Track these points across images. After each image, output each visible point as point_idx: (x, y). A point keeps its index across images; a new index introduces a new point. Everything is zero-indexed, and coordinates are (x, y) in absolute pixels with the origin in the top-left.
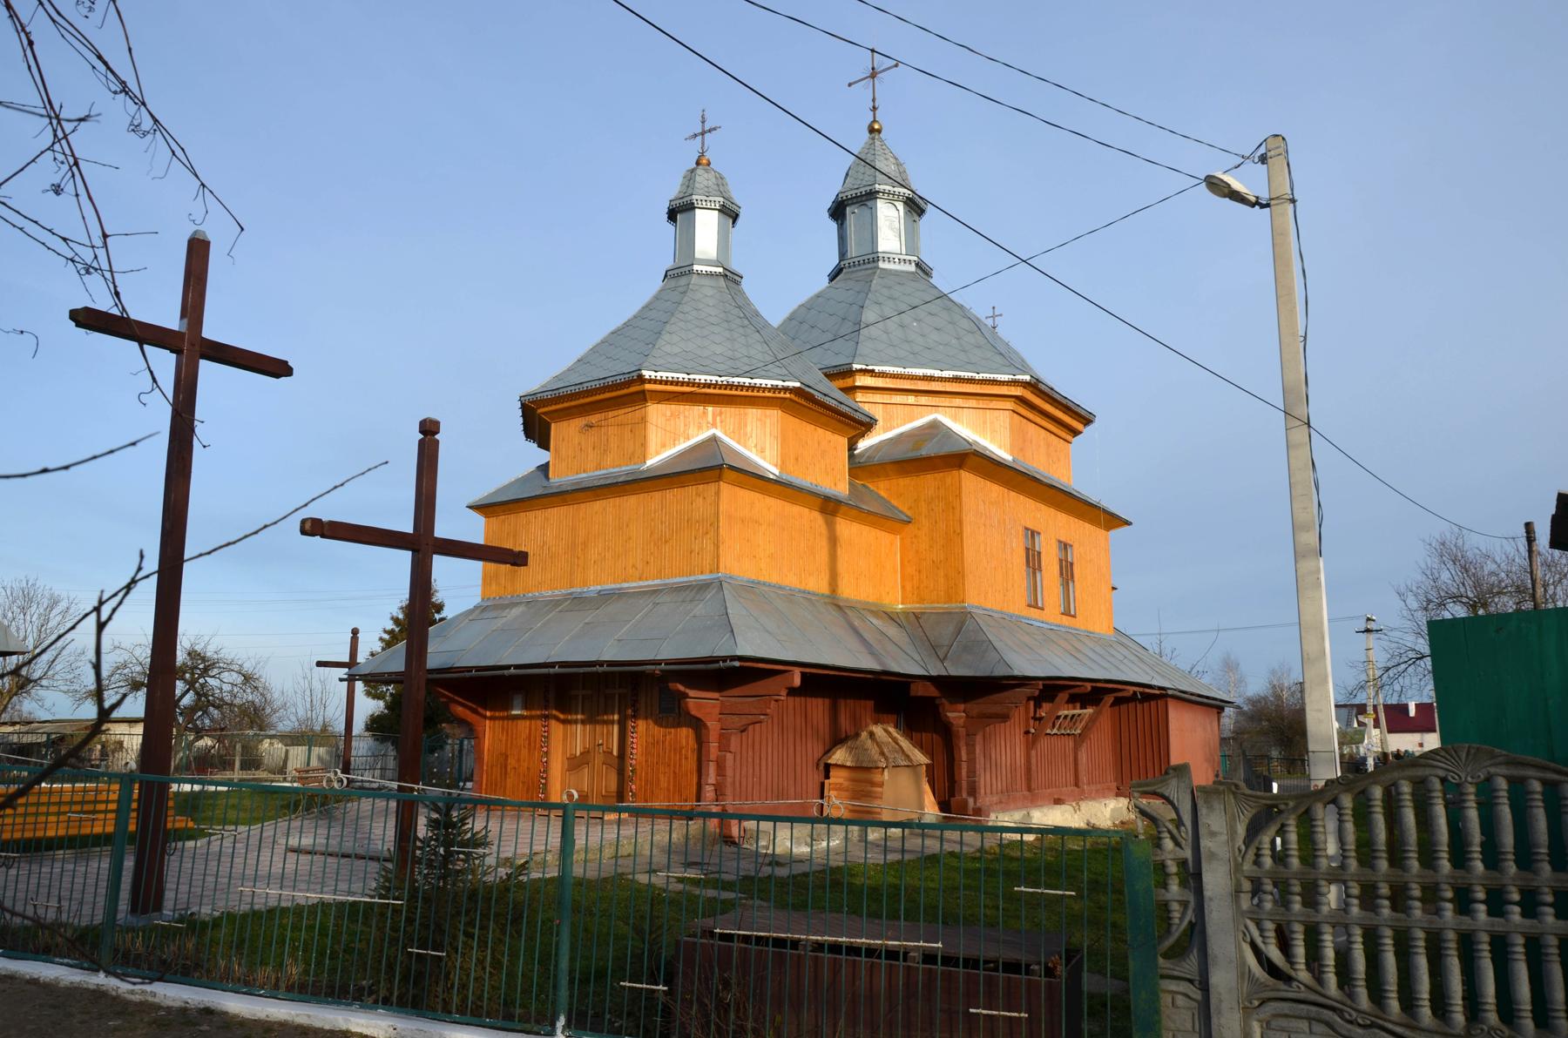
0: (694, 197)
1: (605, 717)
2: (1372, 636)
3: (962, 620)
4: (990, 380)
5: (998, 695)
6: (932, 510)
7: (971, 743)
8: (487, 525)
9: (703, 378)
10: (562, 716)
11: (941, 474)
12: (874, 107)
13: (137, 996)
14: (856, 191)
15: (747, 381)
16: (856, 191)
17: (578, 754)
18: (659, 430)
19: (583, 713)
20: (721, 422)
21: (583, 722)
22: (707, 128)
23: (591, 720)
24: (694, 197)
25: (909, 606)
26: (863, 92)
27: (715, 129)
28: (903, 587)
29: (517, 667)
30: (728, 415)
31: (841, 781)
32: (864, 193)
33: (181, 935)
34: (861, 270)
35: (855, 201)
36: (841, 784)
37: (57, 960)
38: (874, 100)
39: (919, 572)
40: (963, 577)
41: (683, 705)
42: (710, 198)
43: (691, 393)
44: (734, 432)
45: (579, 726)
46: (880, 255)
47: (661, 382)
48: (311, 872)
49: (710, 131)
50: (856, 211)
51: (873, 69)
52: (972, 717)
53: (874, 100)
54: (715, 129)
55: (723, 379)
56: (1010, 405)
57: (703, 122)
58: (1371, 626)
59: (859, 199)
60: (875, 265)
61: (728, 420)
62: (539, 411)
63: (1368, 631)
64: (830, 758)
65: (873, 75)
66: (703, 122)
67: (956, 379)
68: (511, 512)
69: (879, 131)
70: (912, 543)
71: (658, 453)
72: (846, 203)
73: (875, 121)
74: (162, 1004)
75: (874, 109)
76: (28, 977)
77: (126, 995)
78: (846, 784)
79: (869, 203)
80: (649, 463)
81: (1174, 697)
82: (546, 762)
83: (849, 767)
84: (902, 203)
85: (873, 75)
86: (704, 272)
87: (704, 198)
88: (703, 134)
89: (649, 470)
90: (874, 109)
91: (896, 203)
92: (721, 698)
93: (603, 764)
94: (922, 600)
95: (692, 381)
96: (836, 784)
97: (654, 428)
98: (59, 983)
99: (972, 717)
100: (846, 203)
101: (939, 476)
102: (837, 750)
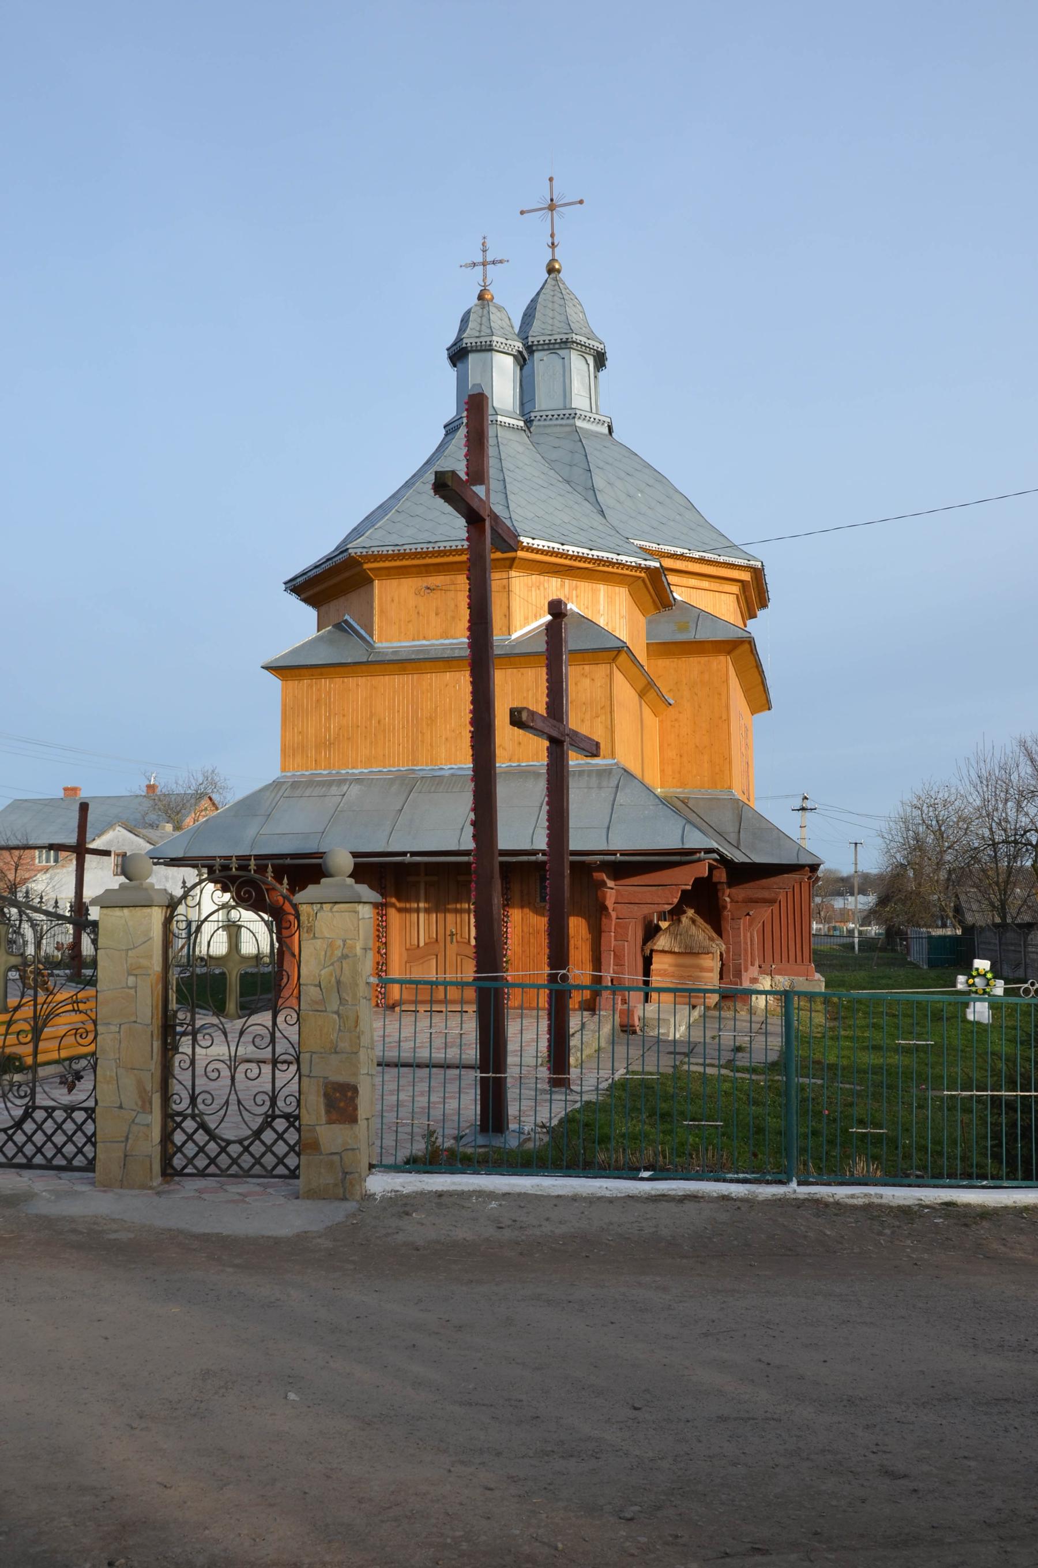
0: (495, 338)
1: (458, 906)
2: (808, 814)
3: (739, 810)
4: (729, 564)
5: (764, 880)
6: (696, 694)
7: (737, 927)
8: (284, 691)
9: (571, 549)
10: (398, 905)
11: (706, 658)
12: (553, 244)
13: (859, 1199)
14: (549, 338)
15: (613, 557)
16: (549, 338)
17: (422, 944)
18: (534, 603)
19: (426, 901)
20: (577, 596)
21: (427, 911)
22: (489, 259)
23: (438, 907)
24: (495, 338)
25: (667, 789)
26: (540, 223)
27: (501, 262)
28: (662, 771)
29: (414, 854)
30: (583, 589)
31: (666, 967)
32: (559, 341)
33: (697, 1151)
34: (556, 425)
35: (546, 347)
36: (665, 970)
37: (730, 1176)
38: (552, 236)
39: (681, 756)
40: (730, 763)
41: (599, 893)
42: (509, 342)
43: (586, 568)
44: (587, 608)
45: (422, 915)
46: (578, 412)
47: (538, 551)
48: (414, 1086)
49: (494, 263)
50: (545, 358)
51: (552, 200)
52: (737, 902)
53: (552, 236)
54: (501, 262)
55: (593, 552)
56: (735, 589)
57: (484, 251)
58: (808, 804)
59: (551, 346)
60: (570, 421)
61: (582, 595)
62: (366, 566)
63: (803, 809)
64: (655, 944)
65: (552, 207)
66: (484, 251)
67: (702, 561)
68: (322, 675)
69: (559, 271)
70: (673, 726)
71: (522, 627)
72: (534, 348)
73: (553, 260)
74: (891, 1204)
75: (553, 245)
76: (715, 1195)
77: (847, 1200)
78: (671, 969)
79: (561, 352)
80: (514, 636)
81: (605, 866)
82: (386, 954)
83: (679, 953)
84: (592, 358)
85: (552, 207)
86: (507, 425)
87: (504, 341)
88: (484, 264)
89: (519, 642)
90: (553, 245)
91: (586, 356)
92: (615, 887)
93: (457, 954)
94: (683, 785)
95: (565, 552)
96: (660, 970)
97: (518, 598)
98: (757, 1197)
99: (737, 902)
100: (534, 348)
101: (704, 660)
102: (660, 936)
